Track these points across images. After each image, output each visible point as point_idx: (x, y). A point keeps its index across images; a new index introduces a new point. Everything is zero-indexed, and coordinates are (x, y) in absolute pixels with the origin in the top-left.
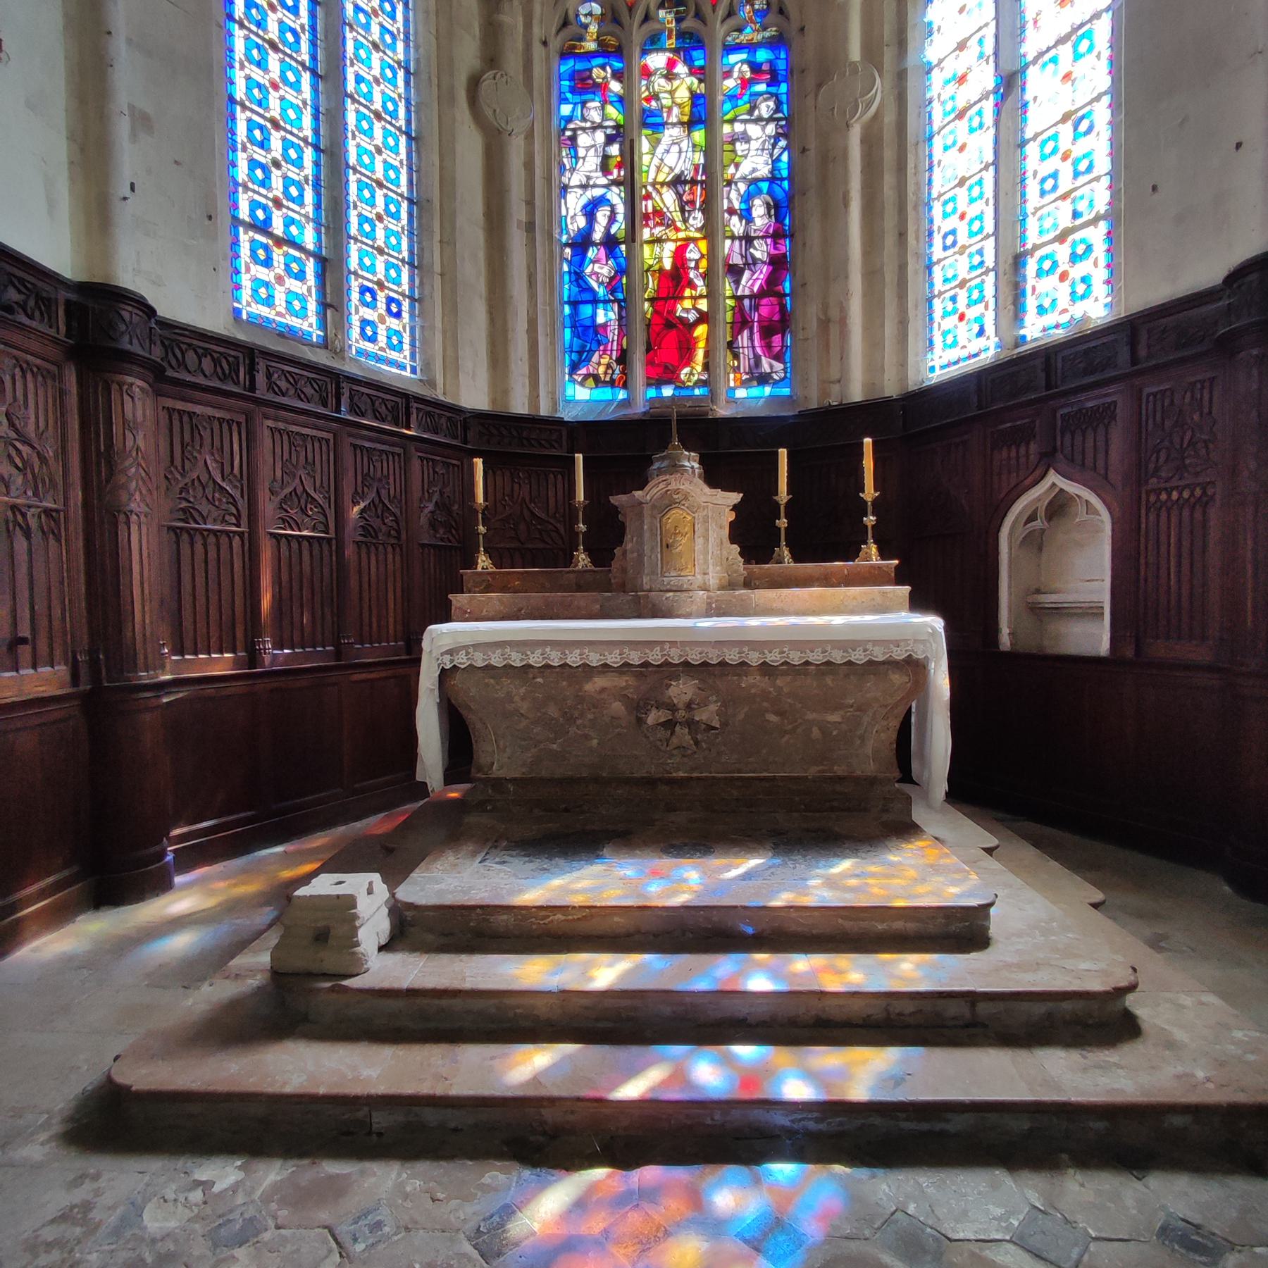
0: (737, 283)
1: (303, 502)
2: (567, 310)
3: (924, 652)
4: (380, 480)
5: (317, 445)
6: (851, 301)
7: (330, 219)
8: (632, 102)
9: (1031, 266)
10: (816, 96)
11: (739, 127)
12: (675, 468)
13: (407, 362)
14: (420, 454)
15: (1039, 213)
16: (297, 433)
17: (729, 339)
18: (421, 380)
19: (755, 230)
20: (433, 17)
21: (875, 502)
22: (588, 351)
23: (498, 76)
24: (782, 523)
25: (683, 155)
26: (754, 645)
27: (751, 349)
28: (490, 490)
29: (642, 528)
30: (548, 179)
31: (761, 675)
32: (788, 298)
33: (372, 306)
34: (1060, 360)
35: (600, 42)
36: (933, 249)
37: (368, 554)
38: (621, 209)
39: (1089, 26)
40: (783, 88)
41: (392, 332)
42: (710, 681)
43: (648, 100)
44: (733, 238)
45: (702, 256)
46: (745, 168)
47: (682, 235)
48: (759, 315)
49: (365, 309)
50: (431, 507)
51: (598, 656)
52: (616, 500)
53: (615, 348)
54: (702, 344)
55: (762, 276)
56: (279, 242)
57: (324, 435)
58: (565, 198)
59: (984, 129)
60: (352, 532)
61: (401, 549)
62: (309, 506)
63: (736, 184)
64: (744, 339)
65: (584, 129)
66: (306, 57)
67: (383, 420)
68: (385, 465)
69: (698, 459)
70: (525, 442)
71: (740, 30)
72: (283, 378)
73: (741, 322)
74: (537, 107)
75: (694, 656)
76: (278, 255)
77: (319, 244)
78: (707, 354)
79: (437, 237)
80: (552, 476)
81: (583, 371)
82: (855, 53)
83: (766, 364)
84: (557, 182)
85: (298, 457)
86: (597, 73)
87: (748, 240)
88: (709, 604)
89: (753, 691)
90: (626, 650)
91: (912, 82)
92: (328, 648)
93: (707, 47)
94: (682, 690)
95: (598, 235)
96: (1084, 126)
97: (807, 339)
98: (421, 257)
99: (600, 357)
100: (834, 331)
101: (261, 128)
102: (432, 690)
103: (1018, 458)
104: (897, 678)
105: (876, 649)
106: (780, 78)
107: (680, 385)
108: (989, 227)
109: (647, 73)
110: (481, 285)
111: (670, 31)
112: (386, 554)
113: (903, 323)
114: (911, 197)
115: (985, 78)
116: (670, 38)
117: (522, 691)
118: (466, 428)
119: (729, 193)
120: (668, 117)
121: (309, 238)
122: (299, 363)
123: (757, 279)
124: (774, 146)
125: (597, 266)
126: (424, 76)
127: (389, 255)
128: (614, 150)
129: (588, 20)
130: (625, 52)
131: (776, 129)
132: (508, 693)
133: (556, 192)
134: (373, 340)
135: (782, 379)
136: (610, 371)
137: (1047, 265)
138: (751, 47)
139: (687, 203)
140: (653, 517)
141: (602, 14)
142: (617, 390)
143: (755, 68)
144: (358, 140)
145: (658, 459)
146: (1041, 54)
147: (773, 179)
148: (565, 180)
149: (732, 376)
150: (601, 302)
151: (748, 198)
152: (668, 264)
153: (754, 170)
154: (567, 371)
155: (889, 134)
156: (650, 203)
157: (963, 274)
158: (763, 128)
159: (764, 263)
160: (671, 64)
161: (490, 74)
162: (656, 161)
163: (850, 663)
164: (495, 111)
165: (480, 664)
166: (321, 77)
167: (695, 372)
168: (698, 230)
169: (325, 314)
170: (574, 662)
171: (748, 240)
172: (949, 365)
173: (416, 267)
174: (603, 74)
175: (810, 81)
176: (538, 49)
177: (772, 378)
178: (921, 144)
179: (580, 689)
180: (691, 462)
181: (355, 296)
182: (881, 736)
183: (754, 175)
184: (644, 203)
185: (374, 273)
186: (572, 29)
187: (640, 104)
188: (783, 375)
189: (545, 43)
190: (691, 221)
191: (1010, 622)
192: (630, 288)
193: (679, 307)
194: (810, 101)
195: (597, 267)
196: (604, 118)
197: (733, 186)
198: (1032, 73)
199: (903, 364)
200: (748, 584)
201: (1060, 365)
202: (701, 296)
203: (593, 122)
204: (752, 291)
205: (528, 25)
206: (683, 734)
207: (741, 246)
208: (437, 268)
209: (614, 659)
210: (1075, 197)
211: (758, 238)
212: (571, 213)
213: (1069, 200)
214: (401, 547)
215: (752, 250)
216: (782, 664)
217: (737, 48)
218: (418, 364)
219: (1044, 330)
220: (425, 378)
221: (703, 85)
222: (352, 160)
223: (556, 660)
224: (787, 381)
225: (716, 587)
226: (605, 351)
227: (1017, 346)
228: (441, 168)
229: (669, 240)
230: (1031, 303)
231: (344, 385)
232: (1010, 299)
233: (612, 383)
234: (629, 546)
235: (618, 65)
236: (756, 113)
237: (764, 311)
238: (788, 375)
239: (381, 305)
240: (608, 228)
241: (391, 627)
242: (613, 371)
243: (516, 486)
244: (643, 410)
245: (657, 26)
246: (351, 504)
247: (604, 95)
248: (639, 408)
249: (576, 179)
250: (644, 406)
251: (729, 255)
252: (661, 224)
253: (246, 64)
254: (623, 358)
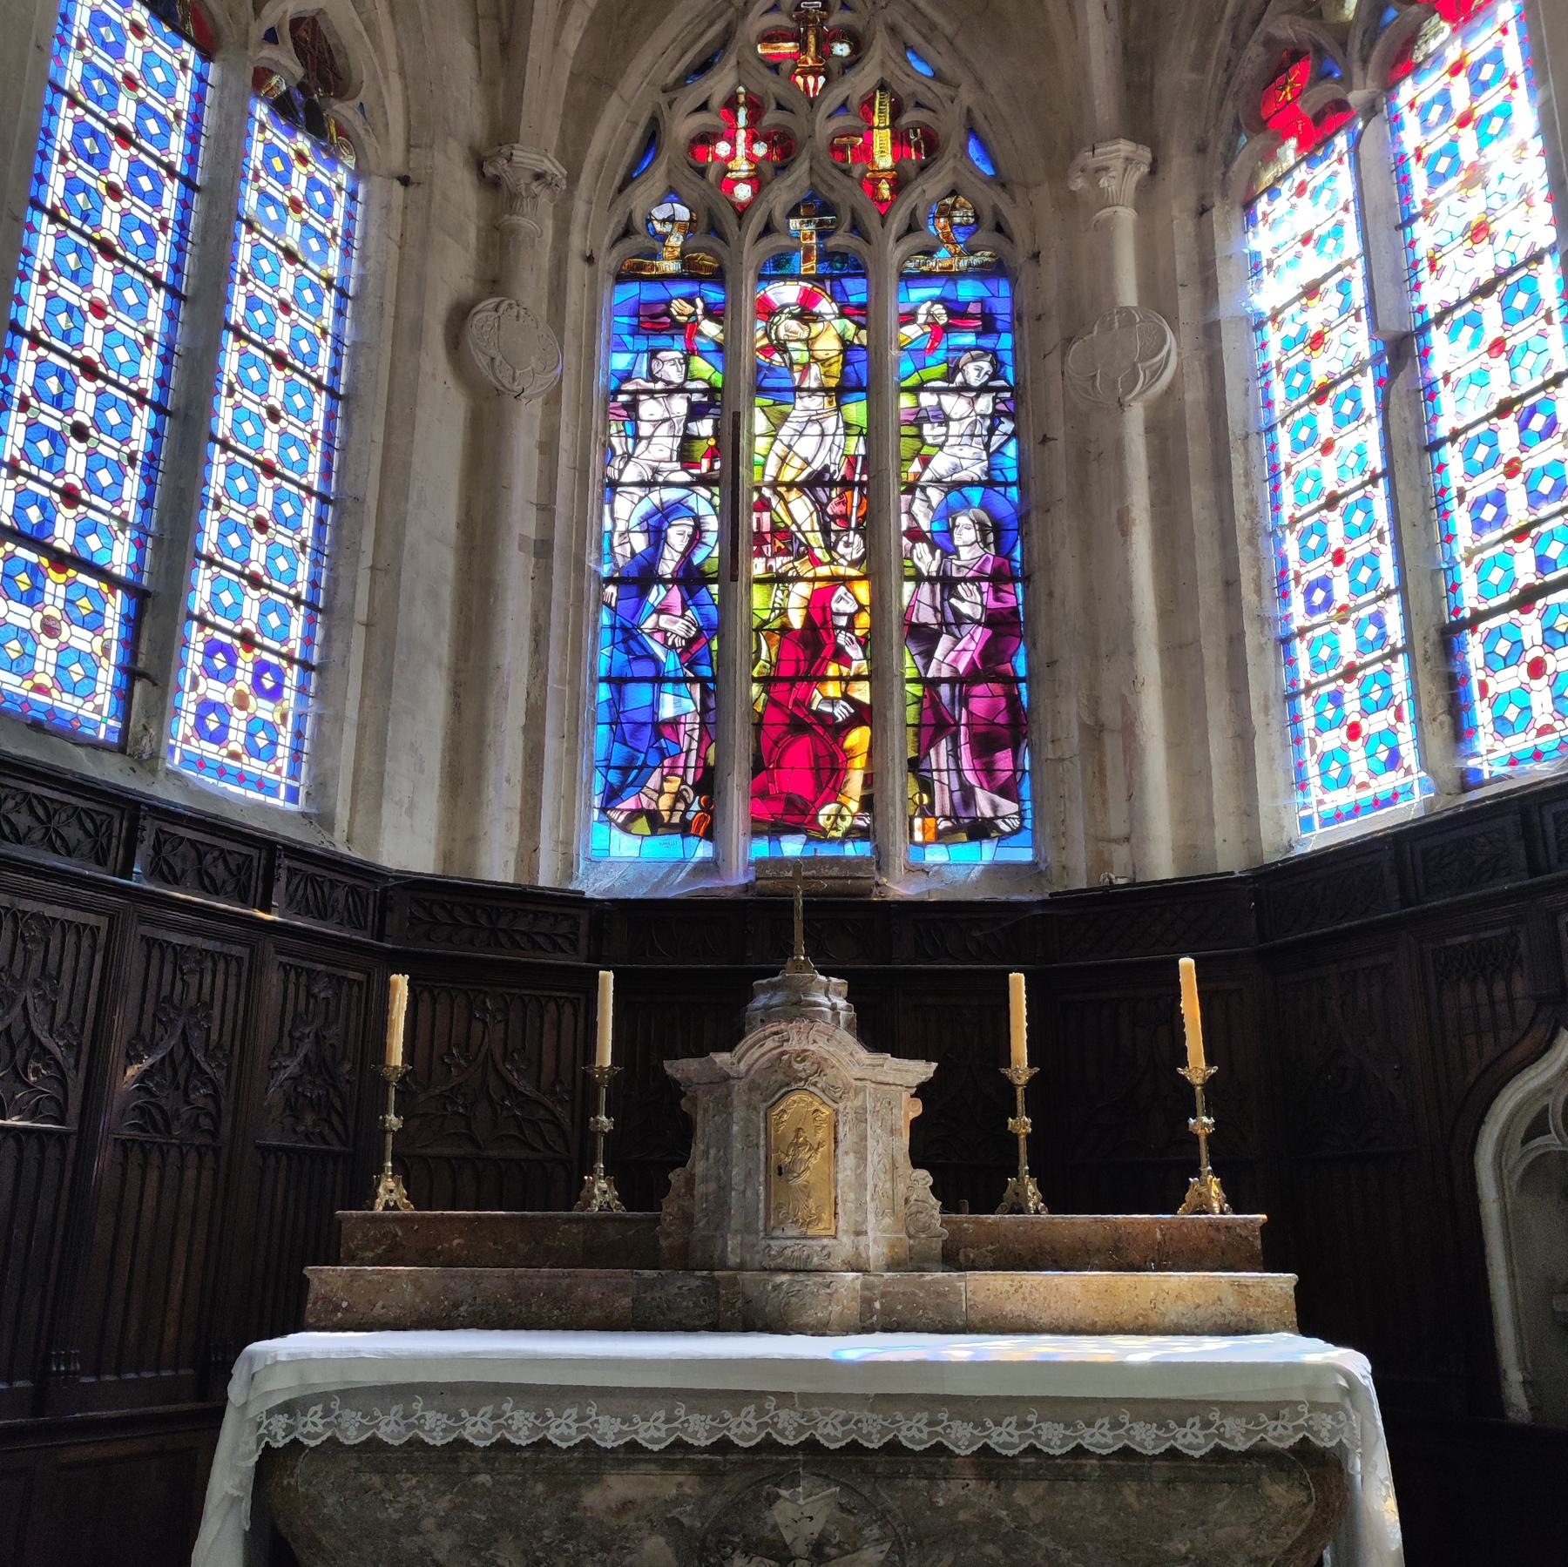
0: (928, 655)
1: (20, 1055)
2: (604, 692)
3: (1333, 1432)
4: (193, 1011)
5: (71, 939)
6: (1143, 697)
7: (167, 524)
8: (738, 356)
9: (1474, 649)
10: (1064, 354)
11: (927, 400)
12: (799, 1009)
13: (283, 782)
14: (285, 959)
15: (1476, 560)
16: (34, 915)
17: (911, 754)
18: (304, 815)
19: (959, 567)
20: (397, 217)
21: (1210, 1083)
22: (641, 768)
23: (504, 306)
24: (1021, 1125)
25: (828, 440)
26: (963, 1406)
27: (954, 775)
28: (423, 1029)
29: (728, 1129)
30: (582, 470)
31: (979, 1478)
32: (1023, 686)
33: (227, 677)
34: (1549, 819)
35: (682, 258)
36: (1291, 610)
37: (144, 1168)
38: (712, 523)
39: (1523, 272)
40: (1006, 341)
41: (257, 724)
42: (866, 1490)
43: (766, 351)
44: (918, 578)
45: (861, 608)
46: (941, 464)
47: (823, 571)
48: (970, 713)
49: (212, 683)
50: (292, 1067)
51: (617, 1425)
52: (681, 1068)
53: (692, 763)
54: (859, 762)
55: (973, 646)
56: (61, 561)
57: (92, 919)
58: (611, 503)
59: (1362, 420)
60: (115, 1122)
61: (217, 1158)
62: (33, 1064)
63: (923, 489)
64: (940, 755)
65: (651, 393)
66: (163, 269)
67: (215, 890)
68: (208, 979)
69: (844, 989)
70: (503, 939)
71: (929, 253)
72: (24, 808)
73: (935, 725)
74: (570, 356)
75: (829, 1430)
76: (55, 586)
77: (137, 567)
78: (868, 781)
79: (366, 561)
80: (552, 1006)
81: (629, 804)
82: (1128, 294)
83: (984, 803)
84: (599, 476)
85: (27, 963)
86: (677, 306)
87: (947, 583)
88: (867, 1302)
89: (963, 1516)
90: (681, 1411)
91: (1230, 342)
92: (18, 1384)
93: (870, 274)
95: (667, 567)
96: (1538, 423)
97: (1061, 760)
98: (331, 594)
99: (664, 779)
100: (1113, 744)
101: (61, 374)
102: (240, 1499)
103: (1492, 1003)
104: (1281, 1494)
105: (1229, 1422)
106: (999, 325)
107: (820, 836)
108: (1389, 577)
109: (767, 310)
110: (443, 648)
111: (808, 250)
112: (182, 1169)
113: (1244, 738)
114: (1242, 523)
115: (1353, 342)
116: (807, 259)
117: (443, 1504)
118: (384, 908)
119: (910, 505)
120: (802, 379)
121: (120, 556)
122: (60, 781)
123: (964, 650)
124: (992, 431)
125: (663, 617)
126: (372, 302)
127: (270, 588)
128: (705, 427)
129: (668, 227)
130: (728, 277)
131: (995, 404)
132: (410, 1507)
133: (594, 490)
134: (219, 738)
135: (1015, 832)
136: (681, 806)
137: (1503, 647)
138: (950, 276)
139: (834, 518)
140: (750, 1106)
141: (691, 220)
142: (693, 841)
143: (957, 312)
144: (238, 397)
145: (764, 989)
146: (1448, 310)
147: (989, 483)
148: (612, 473)
149: (918, 822)
150: (669, 680)
151: (947, 515)
152: (796, 620)
153: (955, 470)
154: (597, 802)
155: (1195, 421)
156: (766, 516)
157: (1348, 655)
158: (973, 402)
159: (978, 623)
160: (808, 300)
161: (491, 302)
162: (779, 448)
163: (1172, 1454)
164: (493, 359)
165: (352, 1437)
166: (184, 298)
167: (845, 811)
168: (853, 564)
169: (130, 690)
170: (563, 1438)
171: (947, 583)
172: (1339, 817)
173: (320, 611)
174: (689, 309)
175: (1053, 333)
176: (576, 270)
177: (997, 828)
178: (1253, 439)
179: (574, 1505)
181: (194, 659)
183: (955, 477)
184: (755, 515)
185: (238, 620)
186: (640, 241)
187: (754, 358)
188: (1016, 823)
189: (590, 260)
190: (841, 548)
191: (1521, 1359)
192: (724, 660)
193: (817, 696)
194: (1053, 363)
195: (664, 621)
196: (688, 376)
197: (918, 493)
198: (1437, 336)
199: (1249, 812)
200: (952, 1258)
201: (1551, 829)
202: (858, 677)
203: (668, 383)
204: (956, 670)
205: (562, 232)
207: (933, 592)
208: (361, 613)
209: (652, 1432)
210: (1539, 536)
211: (964, 580)
212: (621, 527)
213: (1528, 541)
214: (216, 1152)
215: (953, 601)
216: (1025, 1452)
217: (927, 277)
218: (302, 784)
219: (1513, 762)
220: (313, 810)
221: (863, 333)
222: (222, 428)
223: (525, 1432)
224: (1026, 836)
225: (882, 1262)
226: (673, 767)
227: (1465, 788)
228: (387, 447)
229: (799, 578)
230: (1482, 714)
231: (147, 823)
232: (1441, 705)
233: (684, 829)
234: (700, 1167)
235: (715, 295)
236: (959, 378)
237: (978, 706)
238: (1028, 823)
239: (244, 678)
240: (687, 554)
241: (171, 1333)
242: (688, 806)
243: (477, 1027)
244: (743, 881)
245: (784, 242)
246: (123, 1061)
247: (689, 342)
248: (737, 877)
249: (631, 474)
250: (746, 873)
251: (911, 607)
252: (787, 553)
253: (52, 275)
254: (708, 783)
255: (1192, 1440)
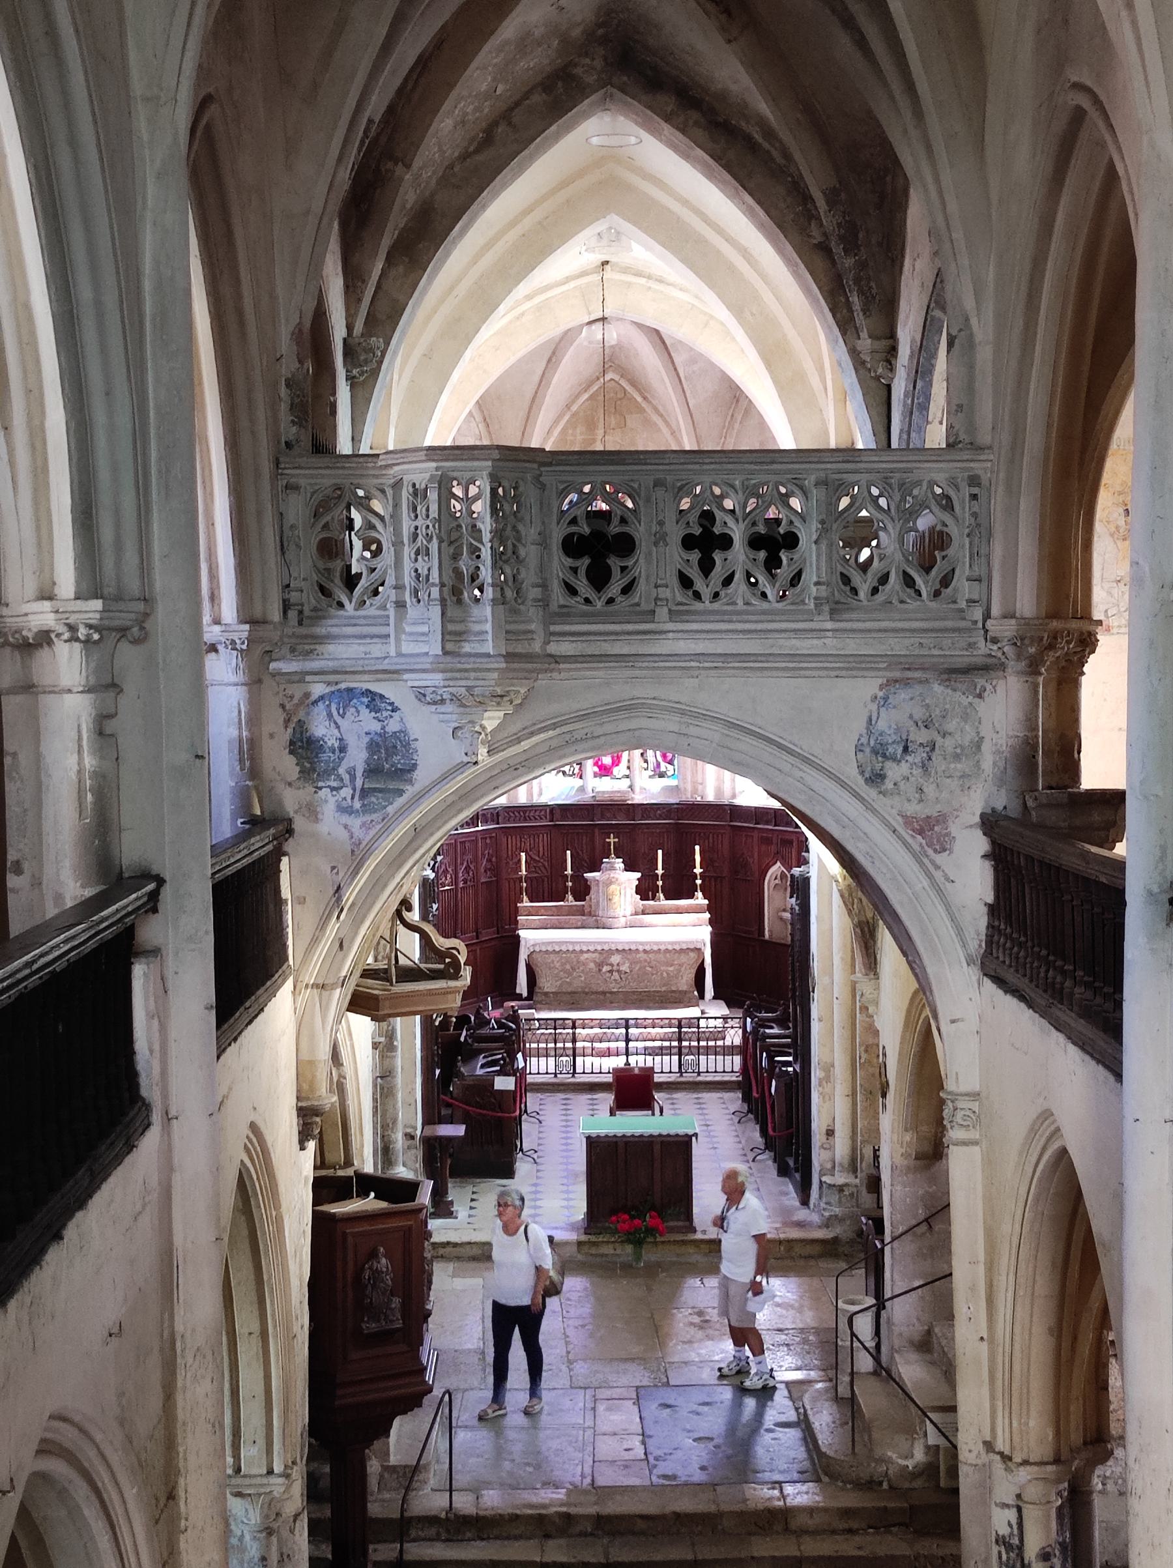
12: (613, 868)
24: (660, 883)
94: (615, 959)
104: (692, 955)
180: (619, 863)
182: (689, 976)
206: (616, 974)
209: (592, 948)
255: (677, 947)
